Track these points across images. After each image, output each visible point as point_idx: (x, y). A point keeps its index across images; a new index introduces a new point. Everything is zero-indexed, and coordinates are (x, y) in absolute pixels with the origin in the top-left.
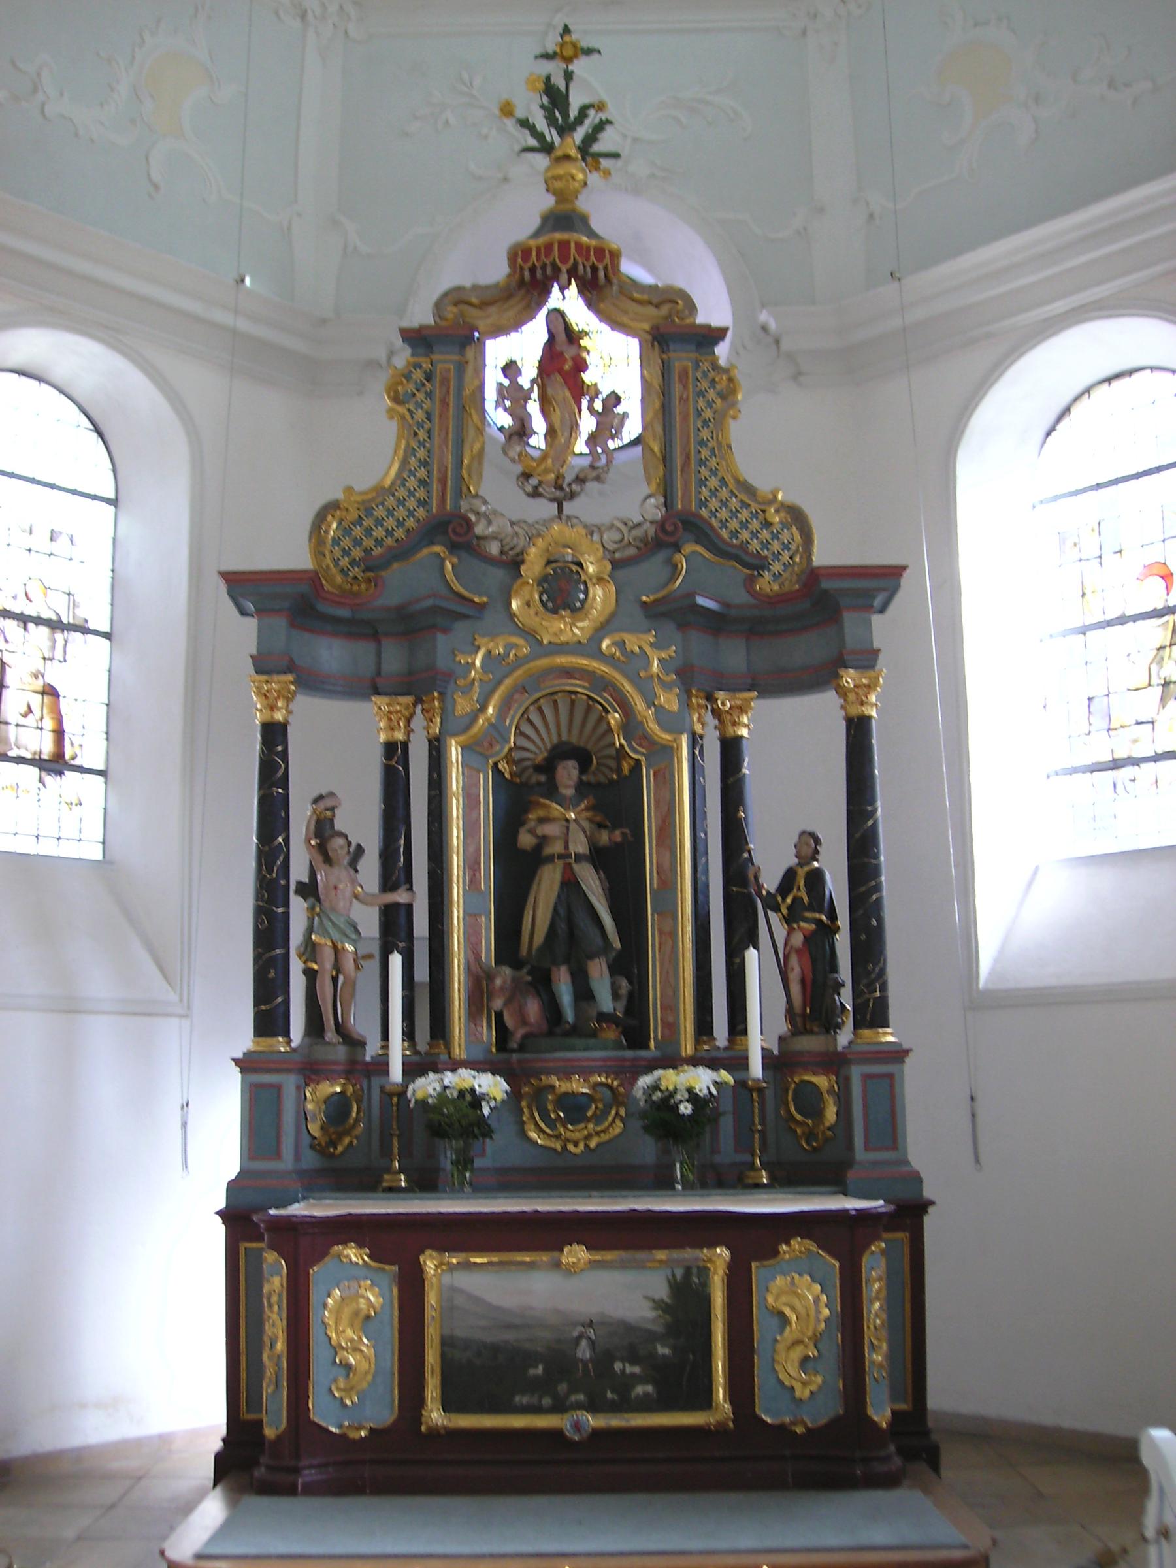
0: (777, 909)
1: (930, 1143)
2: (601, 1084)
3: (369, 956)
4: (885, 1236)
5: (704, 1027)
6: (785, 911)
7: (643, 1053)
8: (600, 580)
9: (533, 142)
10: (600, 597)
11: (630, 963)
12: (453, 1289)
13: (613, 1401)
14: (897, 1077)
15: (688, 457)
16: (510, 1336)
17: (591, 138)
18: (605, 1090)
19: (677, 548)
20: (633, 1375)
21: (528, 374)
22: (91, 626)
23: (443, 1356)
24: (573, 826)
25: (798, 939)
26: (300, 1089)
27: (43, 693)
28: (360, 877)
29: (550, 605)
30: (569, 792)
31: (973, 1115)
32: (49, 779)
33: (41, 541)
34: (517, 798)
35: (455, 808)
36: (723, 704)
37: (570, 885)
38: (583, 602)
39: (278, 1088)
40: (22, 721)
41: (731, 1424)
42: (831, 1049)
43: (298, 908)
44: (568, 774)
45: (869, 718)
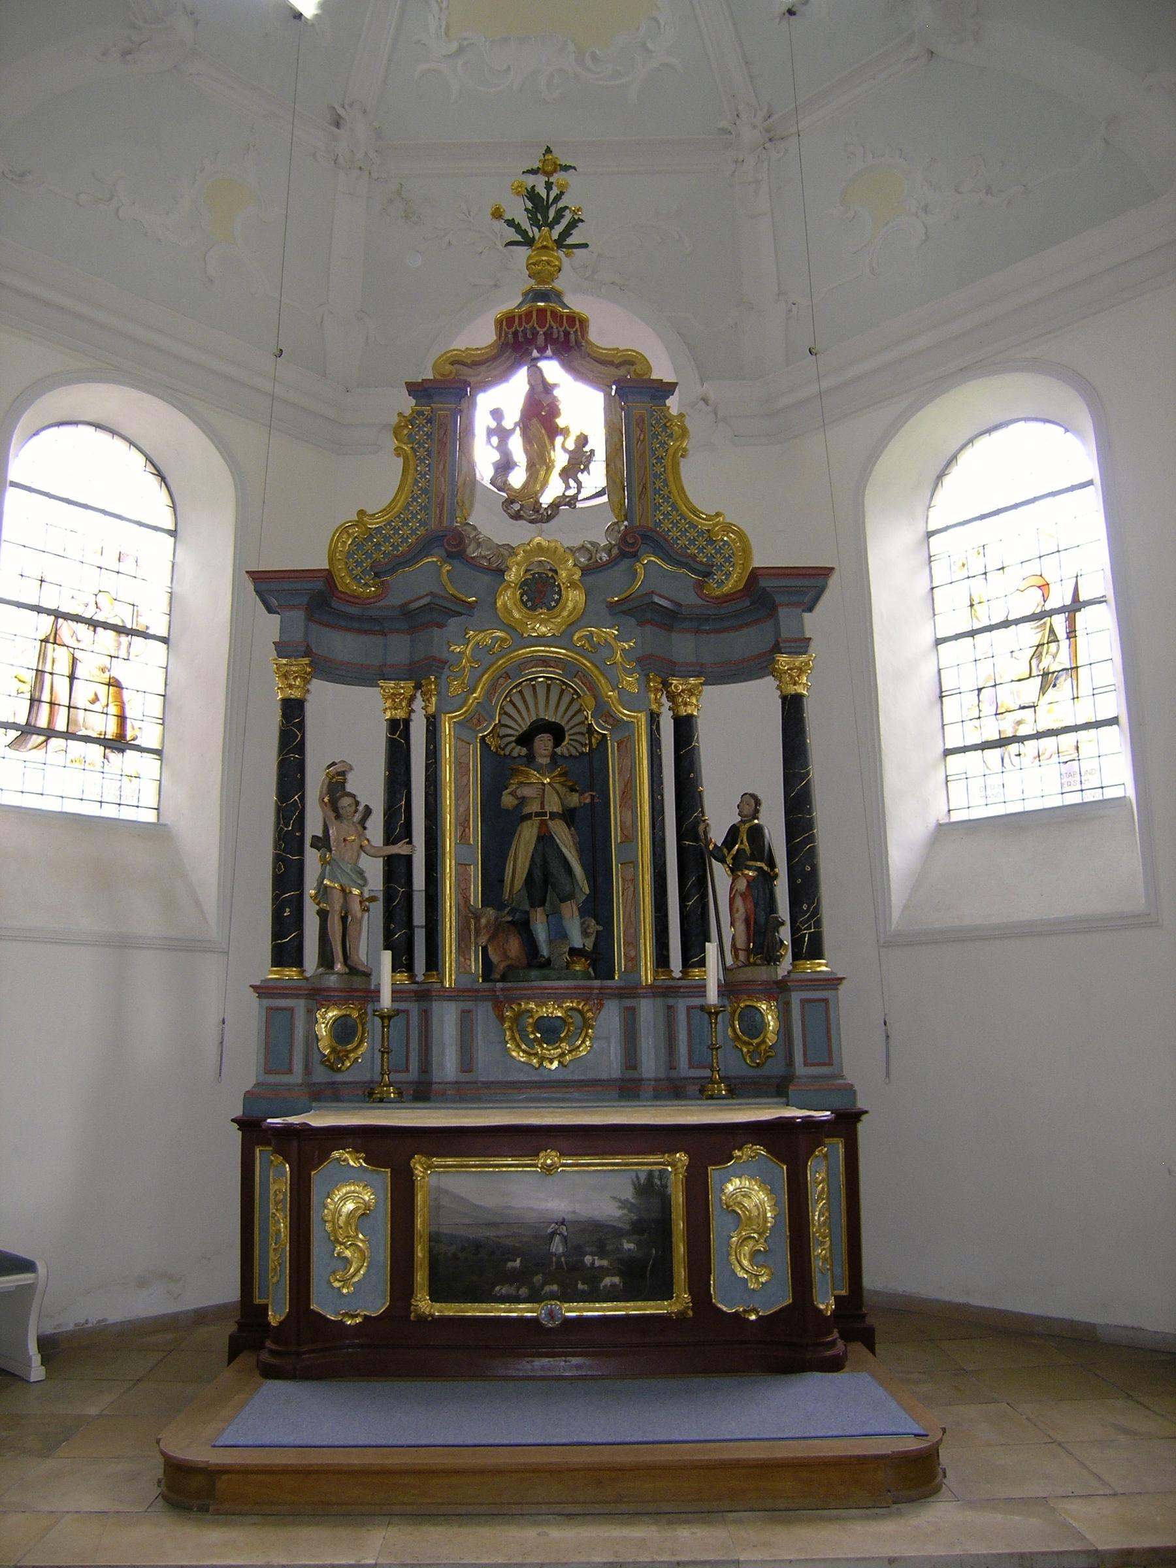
0: (722, 860)
1: (859, 1063)
2: (572, 1009)
3: (373, 899)
4: (827, 1141)
5: (662, 960)
6: (729, 860)
7: (609, 983)
8: (573, 585)
9: (519, 238)
10: (574, 598)
11: (598, 907)
12: (439, 1189)
13: (583, 1291)
14: (831, 1004)
15: (644, 487)
16: (490, 1233)
17: (566, 233)
18: (575, 1014)
19: (635, 556)
20: (601, 1267)
21: (512, 417)
22: (151, 632)
23: (431, 1250)
24: (548, 788)
25: (742, 885)
26: (311, 1012)
27: (109, 684)
28: (368, 833)
29: (529, 604)
30: (544, 761)
31: (888, 1037)
32: (114, 756)
33: (110, 562)
34: (498, 770)
35: (447, 773)
36: (676, 687)
37: (545, 839)
38: (558, 602)
39: (291, 1010)
40: (90, 707)
41: (690, 1313)
42: (774, 977)
43: (312, 857)
44: (543, 743)
45: (801, 696)
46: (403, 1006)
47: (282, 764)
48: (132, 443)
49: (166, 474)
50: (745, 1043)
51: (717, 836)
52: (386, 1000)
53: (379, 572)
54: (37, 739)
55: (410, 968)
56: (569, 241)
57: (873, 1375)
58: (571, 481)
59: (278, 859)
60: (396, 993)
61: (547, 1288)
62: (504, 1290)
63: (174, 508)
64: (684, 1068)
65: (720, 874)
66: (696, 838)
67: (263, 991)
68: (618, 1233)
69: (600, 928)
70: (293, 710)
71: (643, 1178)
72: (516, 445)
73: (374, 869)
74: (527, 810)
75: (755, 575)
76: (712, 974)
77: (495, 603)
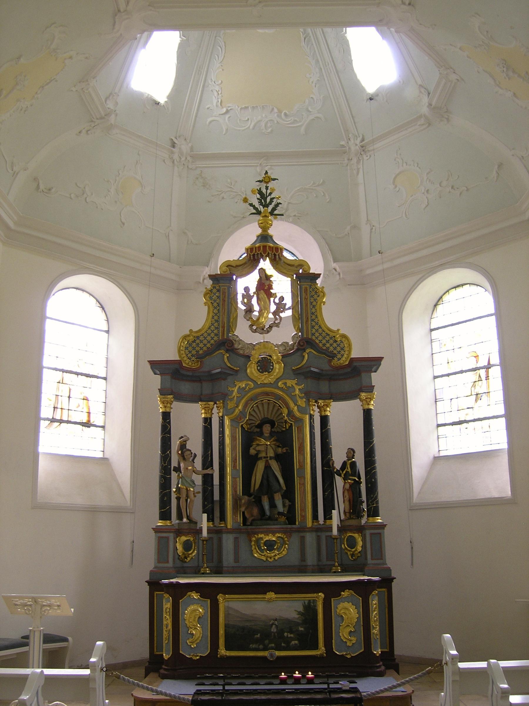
0: (340, 475)
1: (395, 557)
2: (279, 537)
3: (199, 493)
5: (315, 517)
6: (343, 475)
7: (294, 526)
8: (278, 363)
9: (254, 211)
10: (278, 368)
11: (289, 495)
13: (284, 646)
16: (248, 624)
17: (274, 209)
19: (304, 350)
20: (291, 637)
21: (253, 290)
24: (269, 447)
25: (347, 486)
31: (412, 548)
34: (248, 438)
37: (268, 467)
38: (272, 369)
39: (168, 538)
41: (325, 655)
43: (174, 475)
44: (267, 429)
46: (211, 535)
47: (163, 439)
48: (90, 294)
49: (104, 306)
50: (350, 551)
51: (338, 466)
52: (205, 533)
53: (200, 358)
54: (56, 424)
55: (213, 520)
56: (275, 212)
57: (394, 678)
58: (277, 317)
59: (161, 477)
60: (209, 531)
61: (270, 645)
62: (254, 646)
63: (108, 321)
64: (324, 561)
65: (339, 481)
66: (329, 467)
67: (157, 530)
68: (298, 624)
69: (290, 503)
70: (166, 416)
71: (306, 602)
72: (254, 301)
73: (198, 480)
74: (260, 456)
75: (352, 360)
76: (335, 522)
77: (246, 370)
